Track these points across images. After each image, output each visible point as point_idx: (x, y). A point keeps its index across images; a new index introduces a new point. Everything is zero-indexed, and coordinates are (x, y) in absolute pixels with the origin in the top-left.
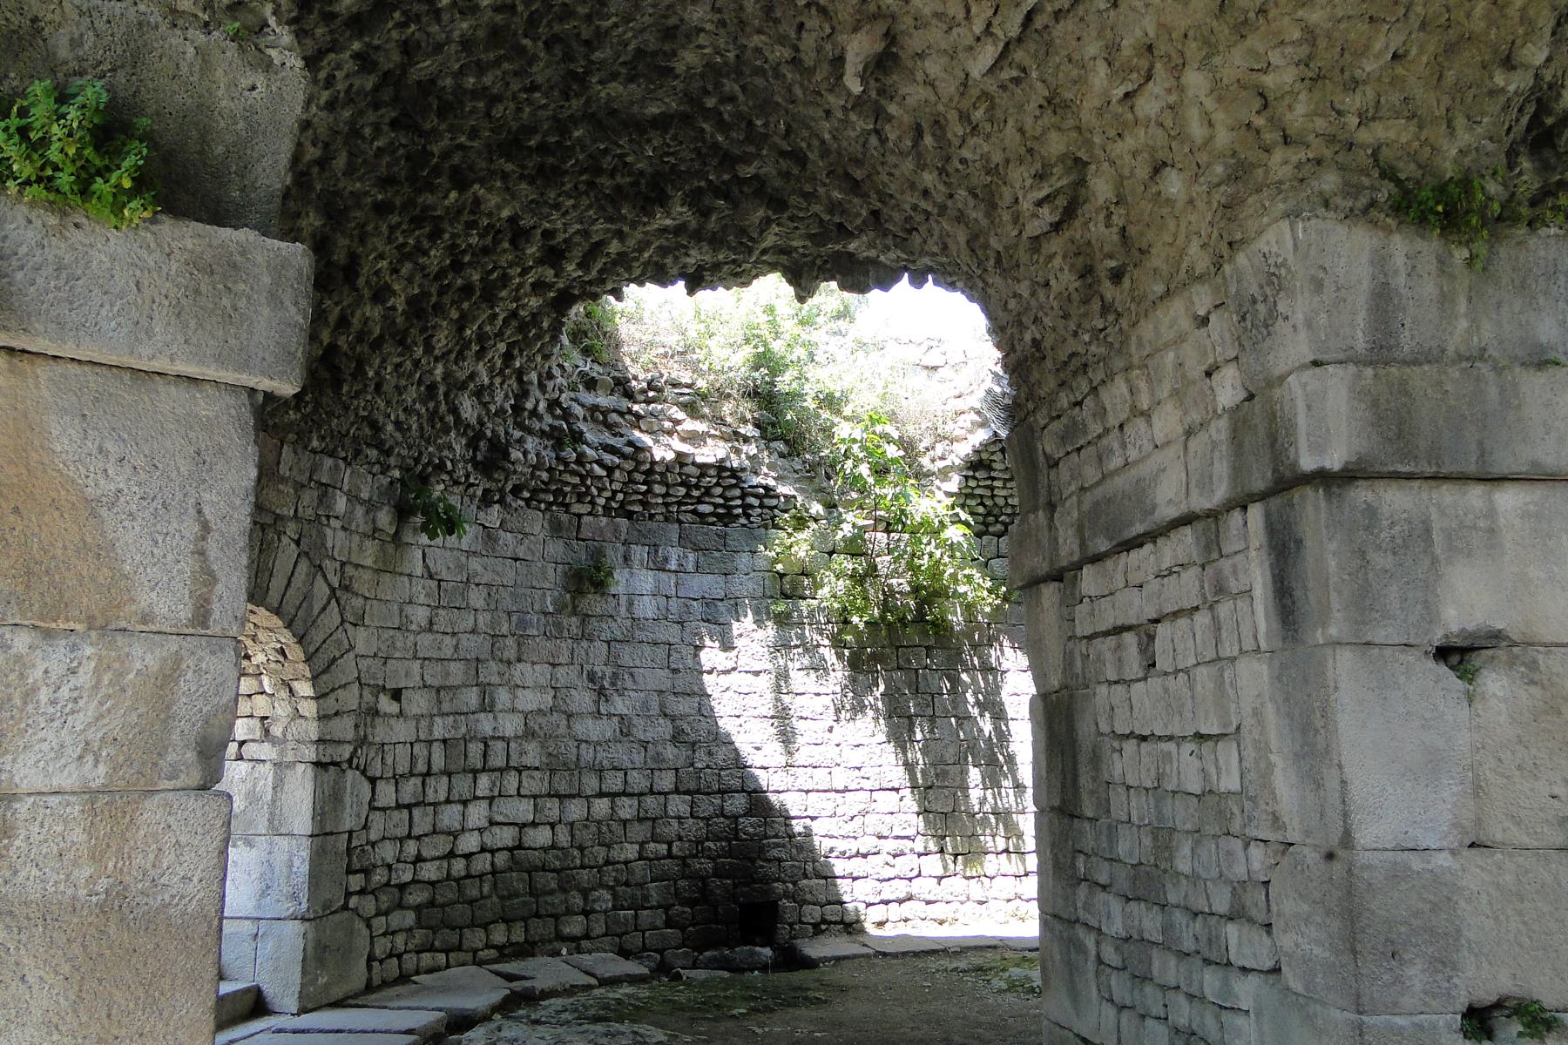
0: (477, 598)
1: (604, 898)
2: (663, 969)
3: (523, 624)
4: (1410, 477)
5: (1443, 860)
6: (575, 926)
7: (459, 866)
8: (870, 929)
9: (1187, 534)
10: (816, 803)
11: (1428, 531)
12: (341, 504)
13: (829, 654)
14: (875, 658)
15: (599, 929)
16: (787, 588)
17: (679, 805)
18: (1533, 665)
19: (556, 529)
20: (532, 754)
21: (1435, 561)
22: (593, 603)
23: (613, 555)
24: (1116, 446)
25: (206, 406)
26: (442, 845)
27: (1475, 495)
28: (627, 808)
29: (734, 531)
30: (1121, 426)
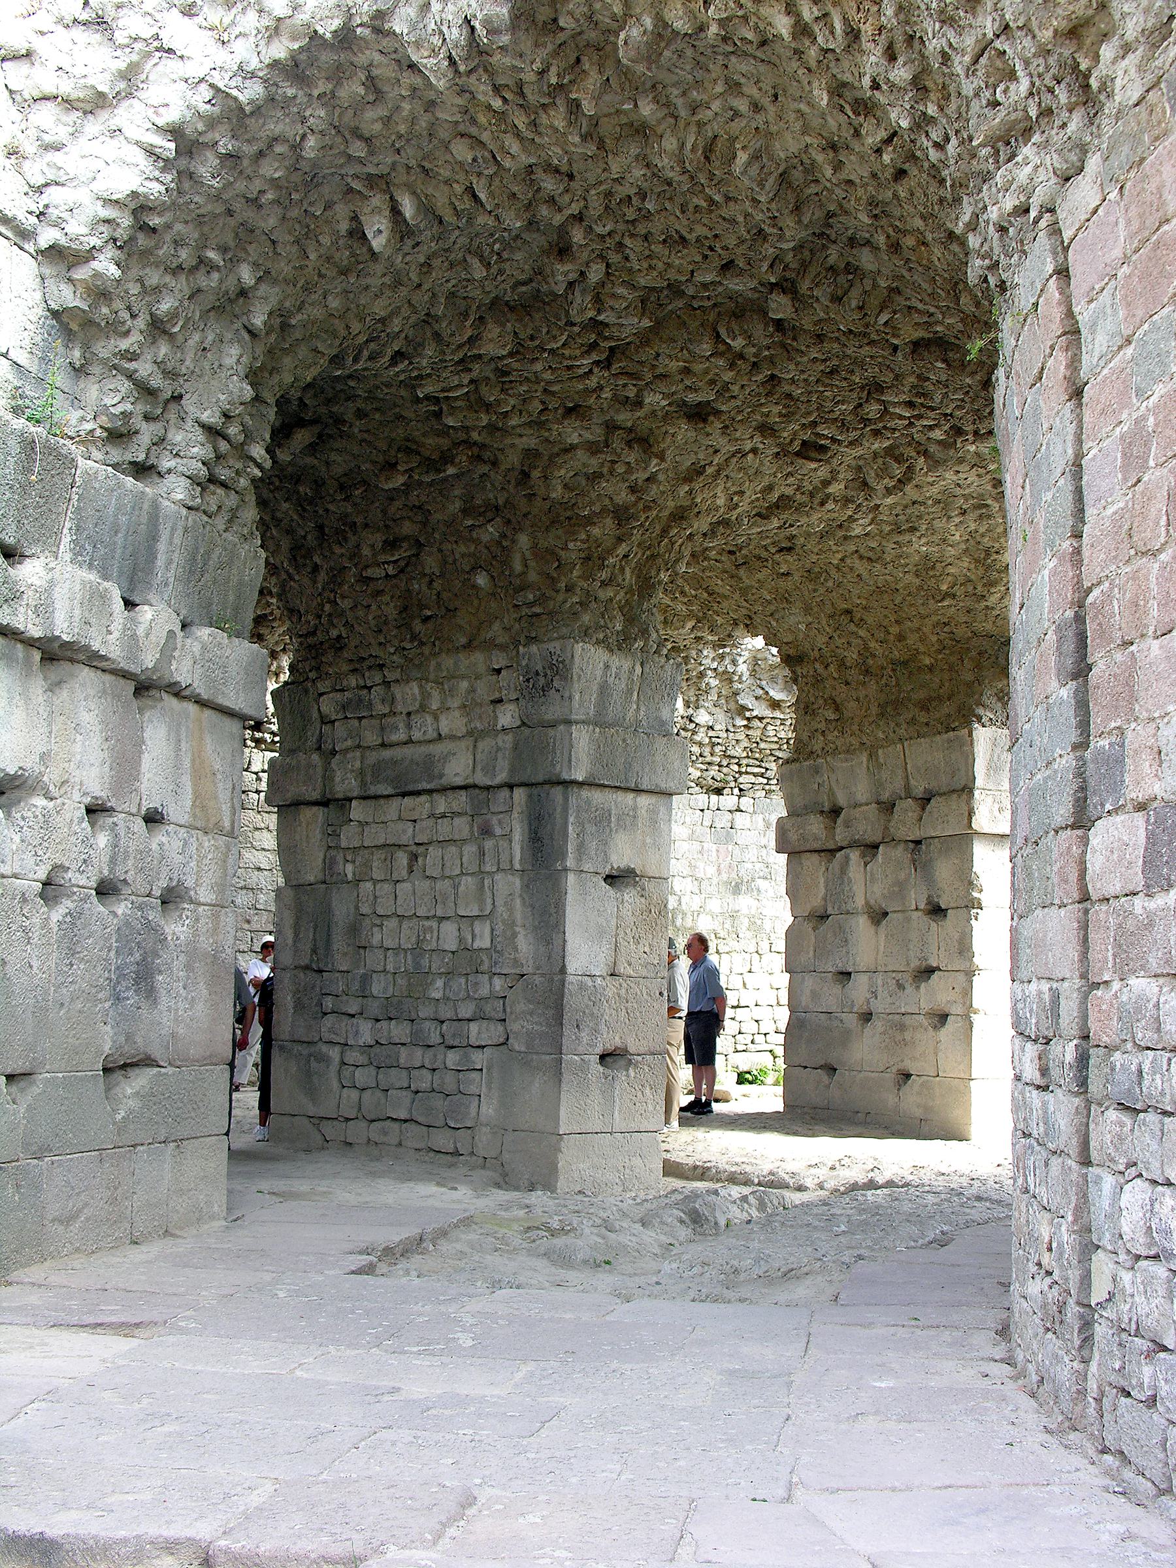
9: (463, 796)
24: (401, 725)
30: (409, 714)
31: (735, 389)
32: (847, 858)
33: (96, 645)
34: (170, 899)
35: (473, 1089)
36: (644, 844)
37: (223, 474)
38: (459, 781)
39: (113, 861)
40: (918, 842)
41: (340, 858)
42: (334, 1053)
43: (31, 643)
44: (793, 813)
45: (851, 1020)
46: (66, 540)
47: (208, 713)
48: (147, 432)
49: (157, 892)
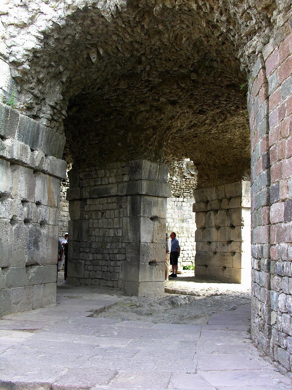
31: (183, 97)
32: (210, 214)
33: (24, 161)
34: (43, 223)
35: (117, 271)
36: (160, 210)
37: (56, 118)
38: (114, 194)
39: (28, 214)
40: (228, 210)
41: (84, 213)
42: (83, 262)
43: (8, 160)
44: (197, 202)
45: (211, 254)
46: (16, 134)
47: (51, 177)
48: (36, 108)
49: (39, 222)
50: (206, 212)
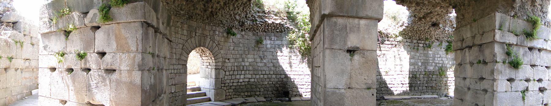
0: (241, 45)
1: (262, 90)
2: (270, 101)
3: (249, 49)
4: (343, 16)
5: (343, 91)
6: (258, 93)
7: (239, 84)
8: (304, 96)
10: (296, 77)
11: (346, 27)
12: (217, 33)
13: (298, 53)
14: (306, 54)
15: (261, 94)
16: (292, 43)
17: (274, 76)
18: (364, 54)
19: (254, 34)
20: (251, 68)
21: (347, 33)
22: (260, 45)
23: (263, 38)
25: (136, 24)
26: (237, 81)
27: (356, 21)
28: (266, 76)
29: (283, 34)
36: (364, 37)
40: (480, 45)
45: (466, 89)
50: (461, 49)
